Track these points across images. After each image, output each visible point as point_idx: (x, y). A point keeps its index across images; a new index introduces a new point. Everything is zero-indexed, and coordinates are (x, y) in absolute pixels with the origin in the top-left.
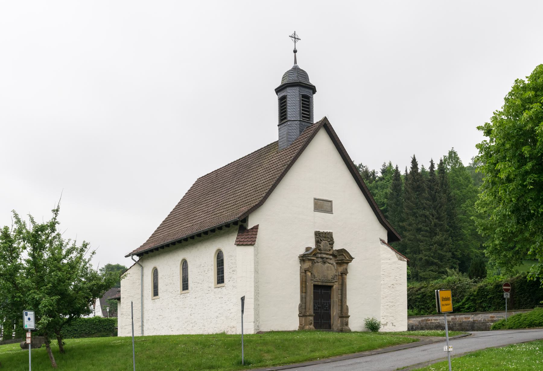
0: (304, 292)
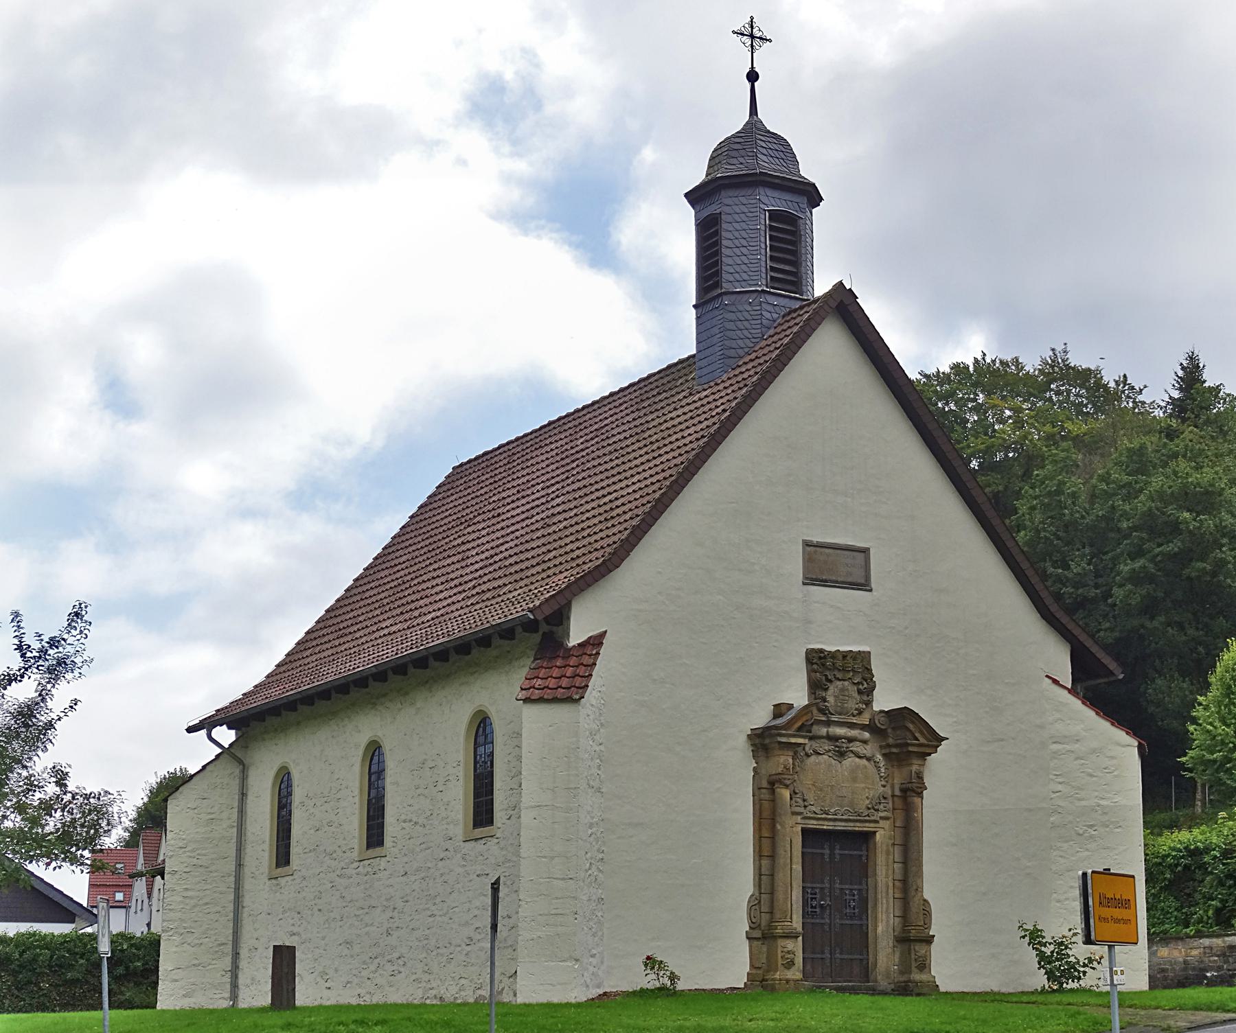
0: (897, 825)
